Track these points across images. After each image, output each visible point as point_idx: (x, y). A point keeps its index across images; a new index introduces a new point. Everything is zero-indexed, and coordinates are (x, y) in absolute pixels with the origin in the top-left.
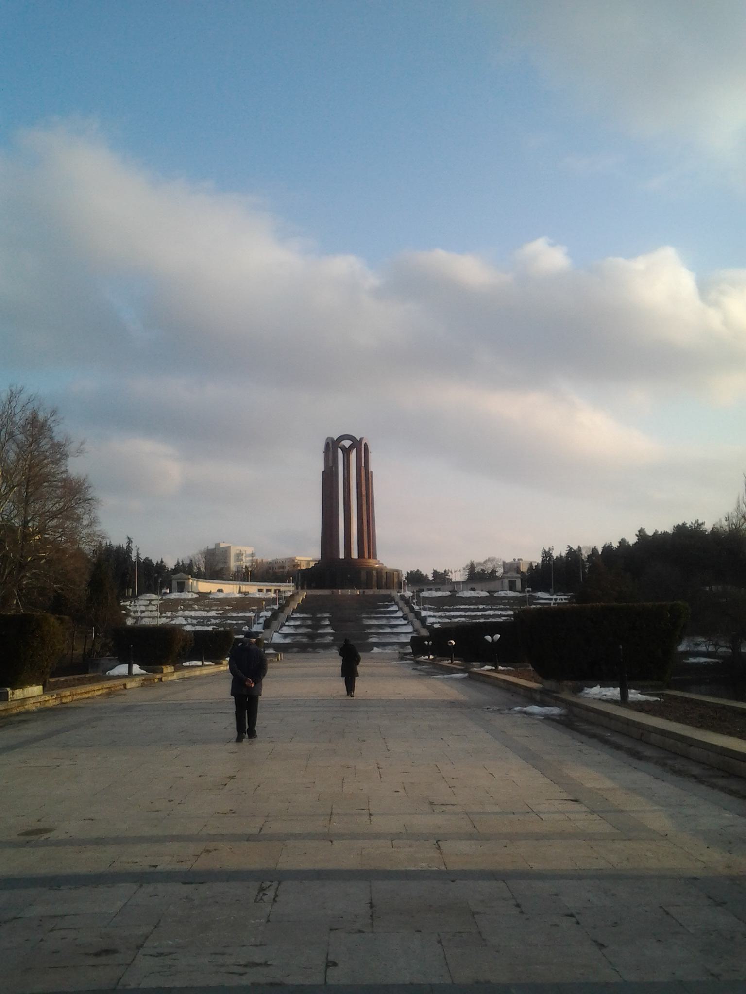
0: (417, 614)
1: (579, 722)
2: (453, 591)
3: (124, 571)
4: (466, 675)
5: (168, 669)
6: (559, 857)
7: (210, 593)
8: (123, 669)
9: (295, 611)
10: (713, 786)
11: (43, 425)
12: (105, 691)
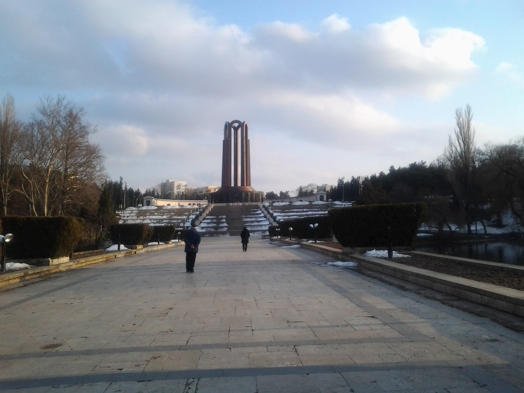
0: (272, 215)
1: (365, 270)
2: (291, 202)
3: (117, 196)
4: (299, 246)
5: (140, 247)
6: (371, 355)
7: (163, 206)
8: (115, 247)
9: (207, 215)
10: (452, 306)
11: (76, 117)
12: (104, 259)
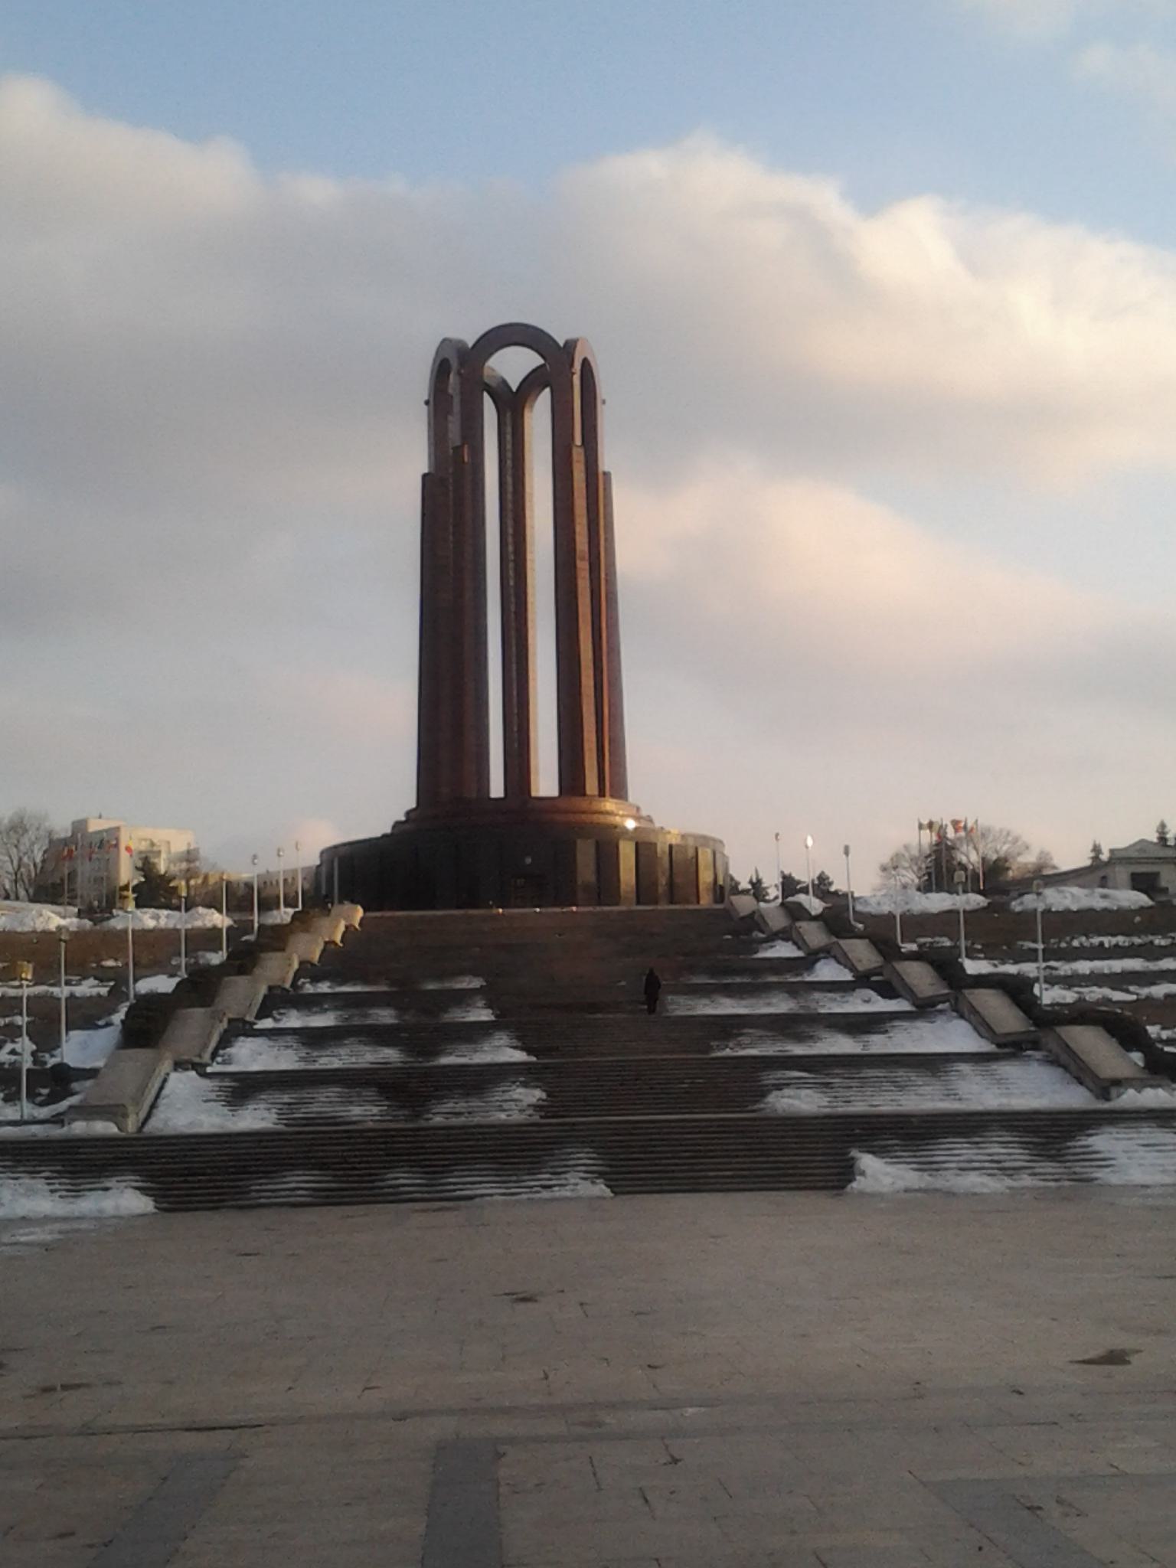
9: (309, 971)
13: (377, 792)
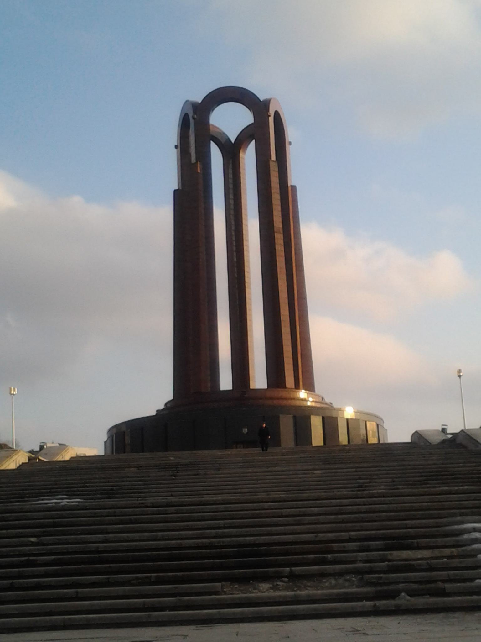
13: (150, 390)
